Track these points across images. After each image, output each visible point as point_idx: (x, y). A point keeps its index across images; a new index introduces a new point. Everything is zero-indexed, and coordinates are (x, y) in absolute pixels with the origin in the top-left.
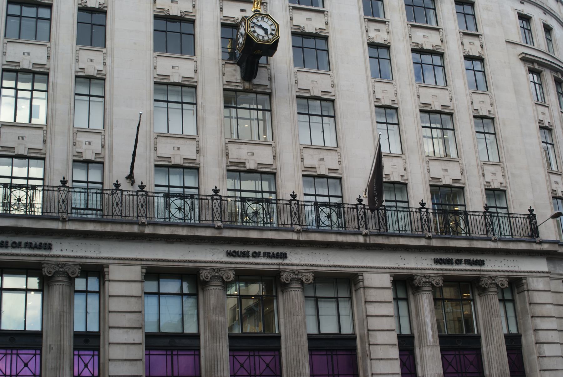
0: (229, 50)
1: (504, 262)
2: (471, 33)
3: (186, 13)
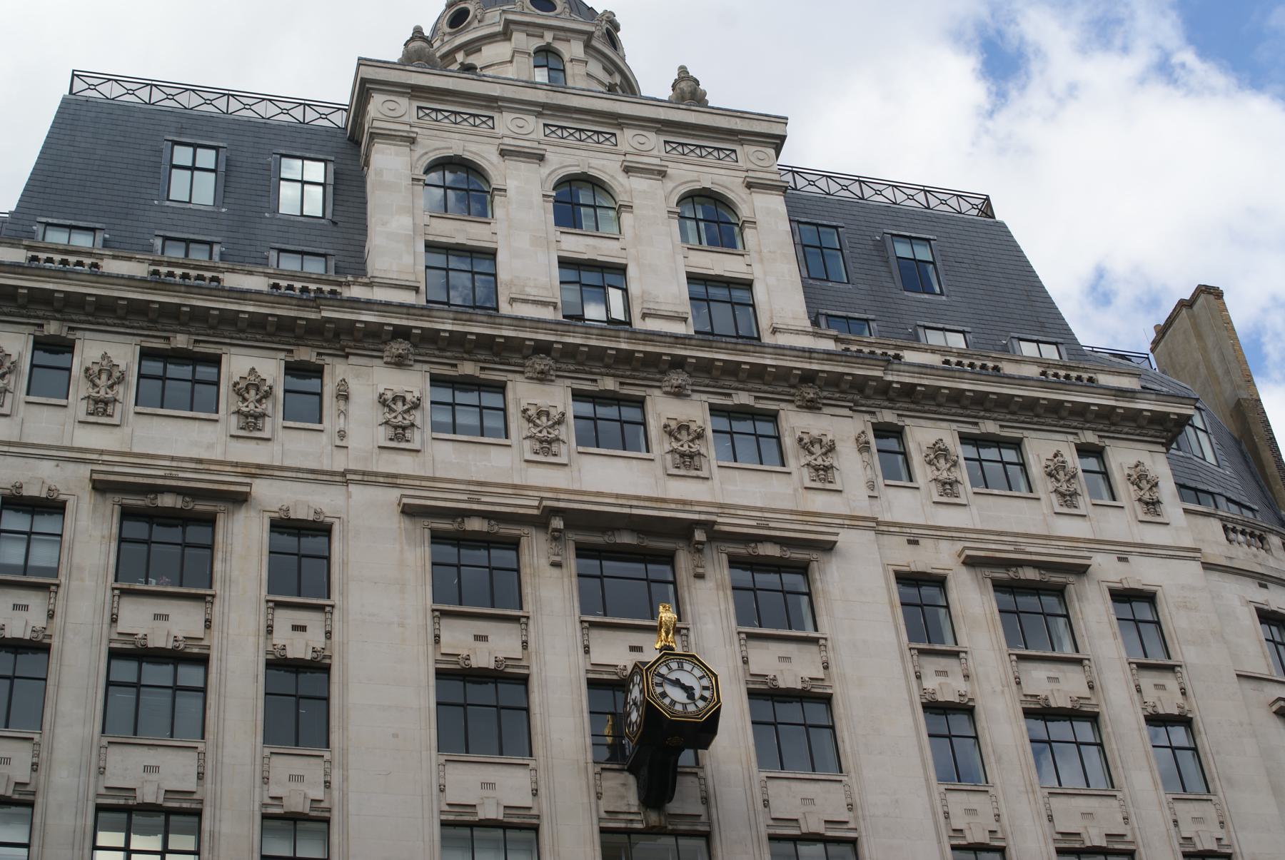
0: (609, 740)
2: (1156, 662)
3: (509, 663)
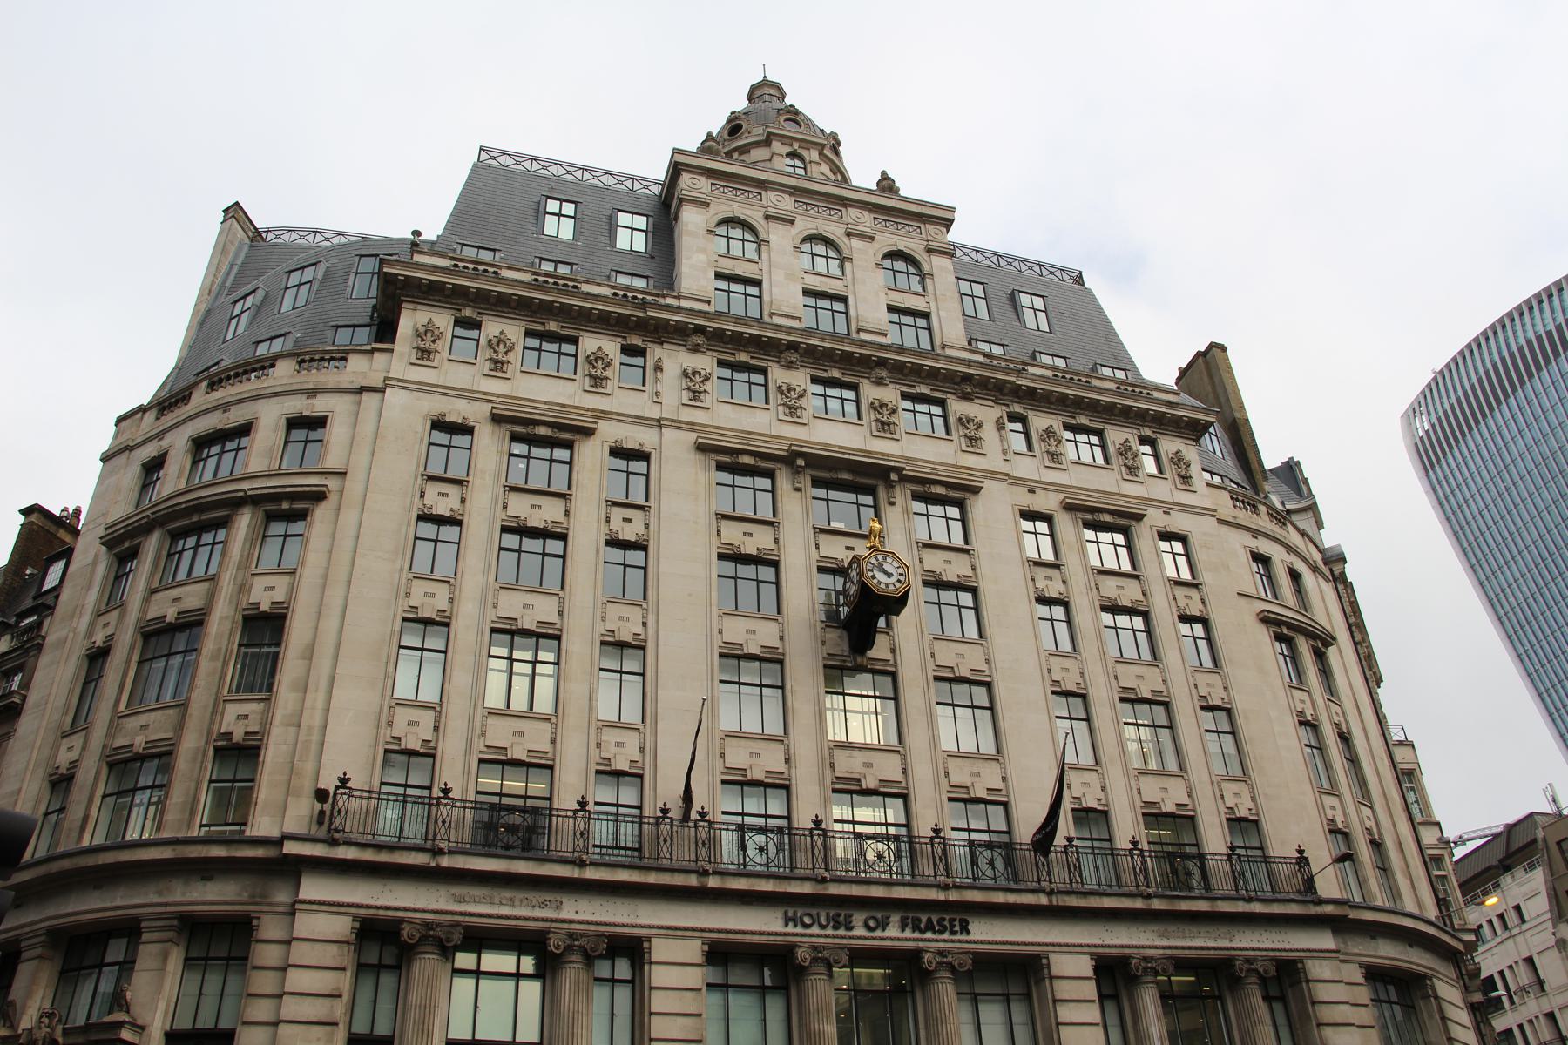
1: (1266, 935)
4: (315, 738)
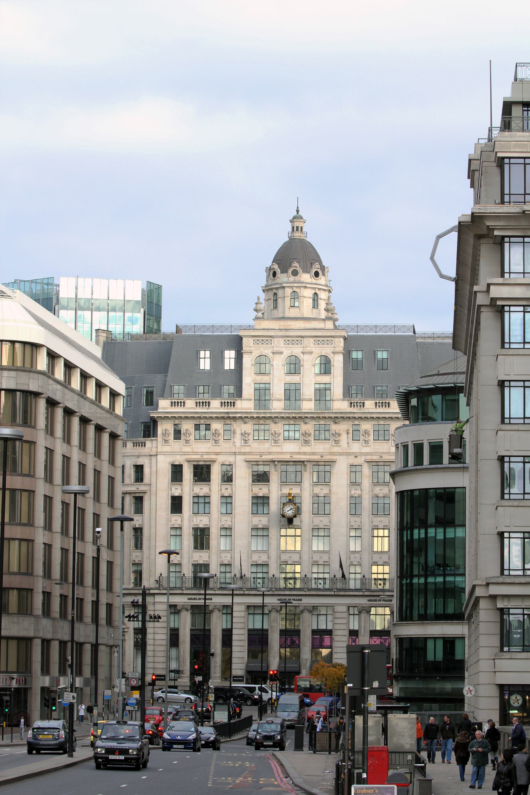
4: (154, 562)
